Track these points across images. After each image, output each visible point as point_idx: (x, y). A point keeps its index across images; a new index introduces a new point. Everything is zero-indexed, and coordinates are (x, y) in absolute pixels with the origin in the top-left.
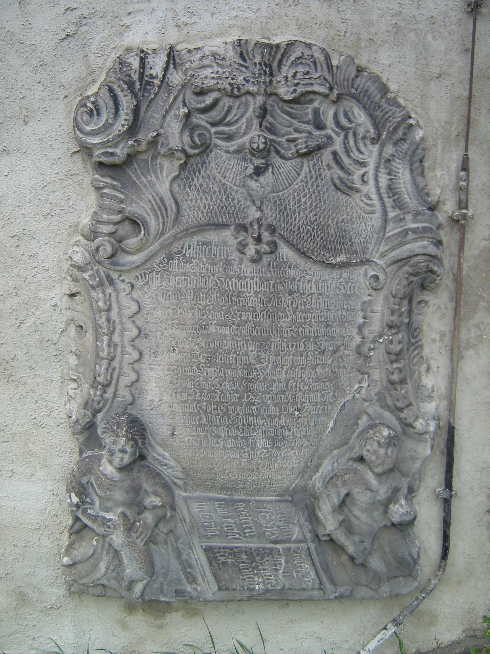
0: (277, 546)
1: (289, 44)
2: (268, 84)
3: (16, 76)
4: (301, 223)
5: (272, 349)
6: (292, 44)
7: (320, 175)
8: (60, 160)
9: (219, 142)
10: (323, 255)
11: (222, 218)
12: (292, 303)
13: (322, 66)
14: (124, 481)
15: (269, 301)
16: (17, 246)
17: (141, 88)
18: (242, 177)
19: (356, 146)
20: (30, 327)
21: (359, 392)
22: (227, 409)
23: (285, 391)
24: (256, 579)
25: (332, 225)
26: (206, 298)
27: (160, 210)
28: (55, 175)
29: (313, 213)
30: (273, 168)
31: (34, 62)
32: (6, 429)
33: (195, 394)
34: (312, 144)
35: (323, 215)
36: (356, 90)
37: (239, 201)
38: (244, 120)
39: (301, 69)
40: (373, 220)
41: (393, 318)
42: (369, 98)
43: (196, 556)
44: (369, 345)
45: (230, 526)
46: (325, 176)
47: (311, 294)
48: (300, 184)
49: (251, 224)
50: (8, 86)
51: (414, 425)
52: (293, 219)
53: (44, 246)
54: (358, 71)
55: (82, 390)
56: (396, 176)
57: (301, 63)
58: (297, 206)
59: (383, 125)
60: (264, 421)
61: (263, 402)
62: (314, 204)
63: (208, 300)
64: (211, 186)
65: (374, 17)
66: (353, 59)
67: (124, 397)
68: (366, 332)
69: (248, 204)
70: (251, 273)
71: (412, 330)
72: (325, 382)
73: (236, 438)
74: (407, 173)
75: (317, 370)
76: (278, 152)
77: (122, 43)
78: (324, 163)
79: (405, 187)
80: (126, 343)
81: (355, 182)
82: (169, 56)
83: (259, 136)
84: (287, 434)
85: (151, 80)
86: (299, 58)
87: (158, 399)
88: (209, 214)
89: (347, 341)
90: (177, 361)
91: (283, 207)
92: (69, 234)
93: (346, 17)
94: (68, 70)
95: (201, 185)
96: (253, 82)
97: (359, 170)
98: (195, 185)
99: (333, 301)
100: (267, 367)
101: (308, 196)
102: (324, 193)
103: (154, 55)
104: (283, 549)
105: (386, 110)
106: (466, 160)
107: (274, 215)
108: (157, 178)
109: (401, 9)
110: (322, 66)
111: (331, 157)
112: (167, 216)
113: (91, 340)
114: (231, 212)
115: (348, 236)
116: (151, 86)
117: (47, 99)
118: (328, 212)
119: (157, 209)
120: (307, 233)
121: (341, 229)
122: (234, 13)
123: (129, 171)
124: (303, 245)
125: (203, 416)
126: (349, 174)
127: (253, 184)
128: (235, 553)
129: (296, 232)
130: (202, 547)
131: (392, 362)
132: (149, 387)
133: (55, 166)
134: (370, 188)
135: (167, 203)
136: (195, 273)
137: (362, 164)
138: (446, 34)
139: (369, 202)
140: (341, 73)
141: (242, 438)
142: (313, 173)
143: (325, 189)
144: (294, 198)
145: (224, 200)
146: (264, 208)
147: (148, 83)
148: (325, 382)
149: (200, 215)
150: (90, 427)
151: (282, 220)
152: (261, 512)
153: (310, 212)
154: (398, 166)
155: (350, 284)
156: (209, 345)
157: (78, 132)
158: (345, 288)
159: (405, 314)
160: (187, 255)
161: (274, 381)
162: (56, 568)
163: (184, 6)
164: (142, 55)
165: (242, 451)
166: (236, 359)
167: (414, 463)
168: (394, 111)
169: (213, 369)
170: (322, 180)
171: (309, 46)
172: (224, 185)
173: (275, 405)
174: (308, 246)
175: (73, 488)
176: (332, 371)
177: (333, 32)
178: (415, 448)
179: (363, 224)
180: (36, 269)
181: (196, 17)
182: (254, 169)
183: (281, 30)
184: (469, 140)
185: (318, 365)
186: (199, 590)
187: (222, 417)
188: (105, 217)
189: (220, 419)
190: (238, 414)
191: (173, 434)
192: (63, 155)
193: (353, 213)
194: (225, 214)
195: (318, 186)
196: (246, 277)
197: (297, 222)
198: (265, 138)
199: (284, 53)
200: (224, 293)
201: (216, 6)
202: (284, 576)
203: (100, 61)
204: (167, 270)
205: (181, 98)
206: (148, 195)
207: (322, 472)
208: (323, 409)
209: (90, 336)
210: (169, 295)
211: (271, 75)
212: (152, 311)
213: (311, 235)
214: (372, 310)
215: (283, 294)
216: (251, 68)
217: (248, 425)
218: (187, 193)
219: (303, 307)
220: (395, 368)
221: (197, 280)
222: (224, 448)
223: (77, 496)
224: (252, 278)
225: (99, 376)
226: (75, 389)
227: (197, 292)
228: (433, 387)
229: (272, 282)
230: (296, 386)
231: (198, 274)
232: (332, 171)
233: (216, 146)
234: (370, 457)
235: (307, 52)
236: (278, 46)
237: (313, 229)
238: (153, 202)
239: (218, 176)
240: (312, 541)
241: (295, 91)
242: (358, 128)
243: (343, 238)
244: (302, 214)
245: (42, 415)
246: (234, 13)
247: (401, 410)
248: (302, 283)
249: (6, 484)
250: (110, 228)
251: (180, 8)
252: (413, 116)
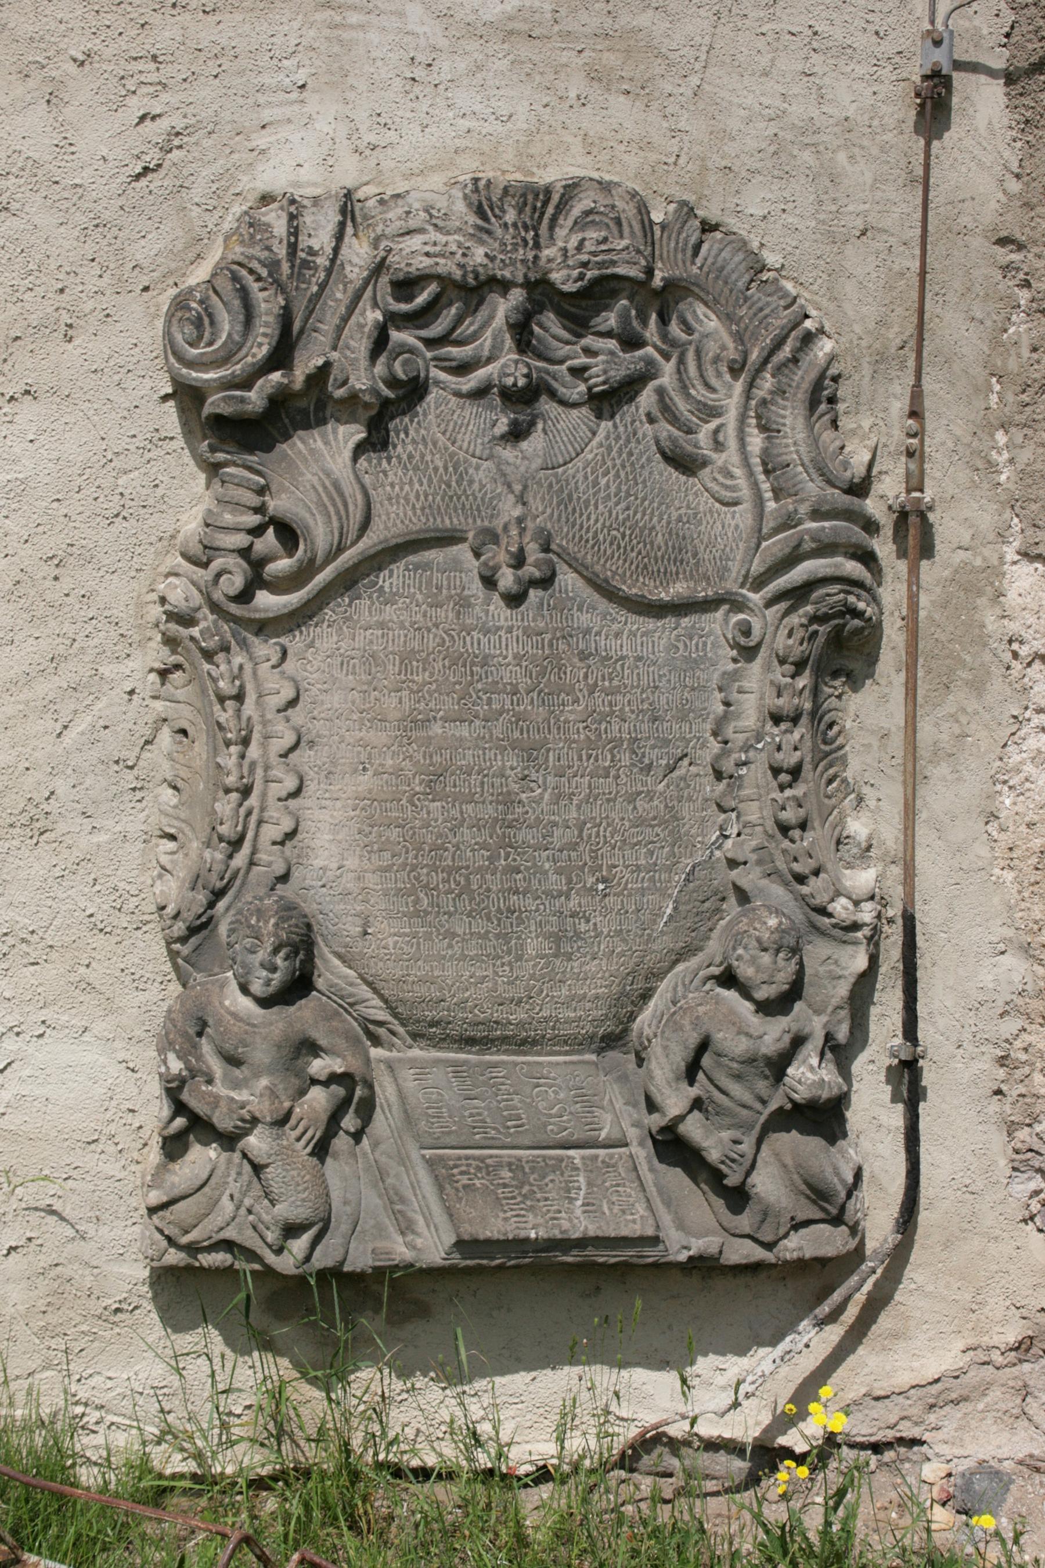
0: (571, 1152)
1: (569, 186)
2: (530, 264)
3: (45, 246)
4: (599, 525)
5: (551, 764)
6: (575, 185)
7: (635, 434)
8: (137, 410)
9: (443, 376)
10: (644, 583)
11: (450, 518)
12: (586, 676)
13: (631, 226)
14: (271, 1024)
15: (542, 673)
16: (56, 578)
17: (292, 273)
18: (486, 440)
19: (702, 376)
20: (83, 733)
21: (719, 848)
22: (468, 879)
23: (577, 844)
24: (531, 1217)
25: (658, 528)
26: (424, 670)
27: (334, 505)
28: (129, 440)
29: (623, 505)
30: (545, 422)
31: (81, 219)
32: (35, 938)
33: (407, 853)
34: (618, 374)
35: (641, 509)
36: (701, 268)
37: (482, 486)
38: (489, 333)
39: (593, 234)
40: (737, 515)
41: (781, 702)
42: (726, 283)
43: (413, 1177)
44: (736, 755)
45: (479, 1114)
46: (645, 436)
47: (622, 658)
48: (595, 451)
49: (506, 528)
50: (31, 266)
51: (830, 908)
52: (584, 517)
53: (108, 576)
54: (704, 231)
55: (186, 855)
56: (779, 431)
57: (592, 222)
58: (591, 492)
59: (753, 334)
60: (538, 902)
61: (535, 865)
62: (624, 488)
63: (427, 674)
64: (428, 458)
65: (734, 124)
66: (692, 209)
67: (269, 864)
68: (729, 732)
69: (499, 491)
70: (506, 619)
71: (823, 726)
72: (653, 826)
73: (485, 936)
74: (800, 423)
75: (638, 803)
76: (553, 394)
77: (252, 185)
78: (641, 410)
79: (797, 452)
80: (274, 759)
81: (702, 444)
82: (343, 211)
83: (516, 362)
84: (583, 927)
85: (310, 258)
86: (588, 213)
87: (335, 866)
88: (427, 511)
89: (694, 748)
90: (370, 791)
91: (564, 495)
92: (157, 553)
93: (679, 127)
94: (150, 236)
95: (410, 457)
96: (502, 261)
97: (707, 422)
98: (398, 457)
99: (665, 671)
100: (542, 798)
101: (613, 472)
102: (643, 467)
103: (314, 209)
104: (583, 1158)
105: (760, 305)
106: (917, 394)
107: (549, 511)
108: (327, 443)
109: (786, 105)
110: (631, 226)
111: (654, 398)
112: (348, 516)
113: (204, 756)
114: (468, 507)
115: (689, 548)
116: (310, 269)
117: (108, 293)
118: (652, 502)
119: (328, 504)
120: (611, 544)
121: (677, 534)
122: (465, 124)
123: (270, 428)
124: (604, 566)
125: (422, 895)
126: (689, 431)
127: (507, 453)
128: (488, 1166)
129: (591, 542)
130: (423, 1156)
131: (782, 788)
132: (317, 843)
133: (128, 422)
134: (731, 456)
135: (347, 491)
136: (402, 622)
137: (711, 412)
138: (875, 151)
139: (729, 482)
140: (669, 238)
141: (498, 936)
142: (621, 429)
143: (644, 460)
144: (586, 478)
145: (454, 484)
146: (529, 497)
147: (305, 264)
148: (653, 826)
149: (410, 513)
150: (200, 927)
151: (563, 519)
152: (538, 1086)
153: (617, 504)
154: (782, 412)
155: (696, 638)
156: (431, 757)
157: (172, 360)
158: (686, 645)
159: (807, 692)
160: (387, 590)
161: (555, 824)
162: (129, 1223)
163: (369, 112)
164: (292, 209)
165: (499, 963)
166: (482, 783)
167: (834, 987)
168: (773, 306)
169: (439, 804)
170: (638, 442)
171: (606, 187)
172: (452, 455)
173: (559, 872)
174: (614, 568)
175: (170, 1044)
176: (666, 806)
177: (653, 157)
178: (835, 957)
179: (719, 524)
180: (94, 622)
181: (392, 132)
182: (509, 425)
183: (554, 157)
184: (925, 354)
185: (639, 793)
186: (419, 1246)
187: (459, 896)
188: (228, 518)
189: (454, 899)
190: (489, 890)
191: (366, 933)
192: (143, 401)
193: (698, 504)
194: (456, 510)
195: (630, 454)
196: (499, 628)
197: (592, 522)
198: (528, 365)
199: (560, 203)
200: (456, 660)
201: (430, 110)
202: (585, 1212)
203: (211, 220)
204: (347, 619)
205: (368, 293)
206: (309, 476)
207: (656, 1005)
208: (652, 880)
209: (200, 749)
210: (354, 666)
211: (537, 246)
212: (321, 697)
213: (619, 548)
214: (740, 687)
215: (569, 660)
216: (499, 232)
217: (509, 910)
218: (385, 473)
219: (607, 683)
220: (788, 798)
221: (406, 636)
222: (463, 957)
223: (179, 1057)
224: (510, 630)
225: (221, 824)
226: (173, 853)
227: (406, 658)
228: (870, 837)
229: (547, 637)
230: (598, 835)
231: (407, 624)
232: (656, 425)
233: (437, 383)
234: (745, 971)
235: (603, 200)
236: (548, 191)
237: (623, 536)
238: (320, 489)
239: (442, 439)
240: (641, 1144)
241: (581, 277)
242: (705, 341)
243: (680, 550)
244: (601, 507)
245: (105, 907)
246: (465, 124)
247: (801, 879)
248: (603, 637)
249: (30, 1051)
250: (241, 540)
251: (362, 116)
252: (813, 313)
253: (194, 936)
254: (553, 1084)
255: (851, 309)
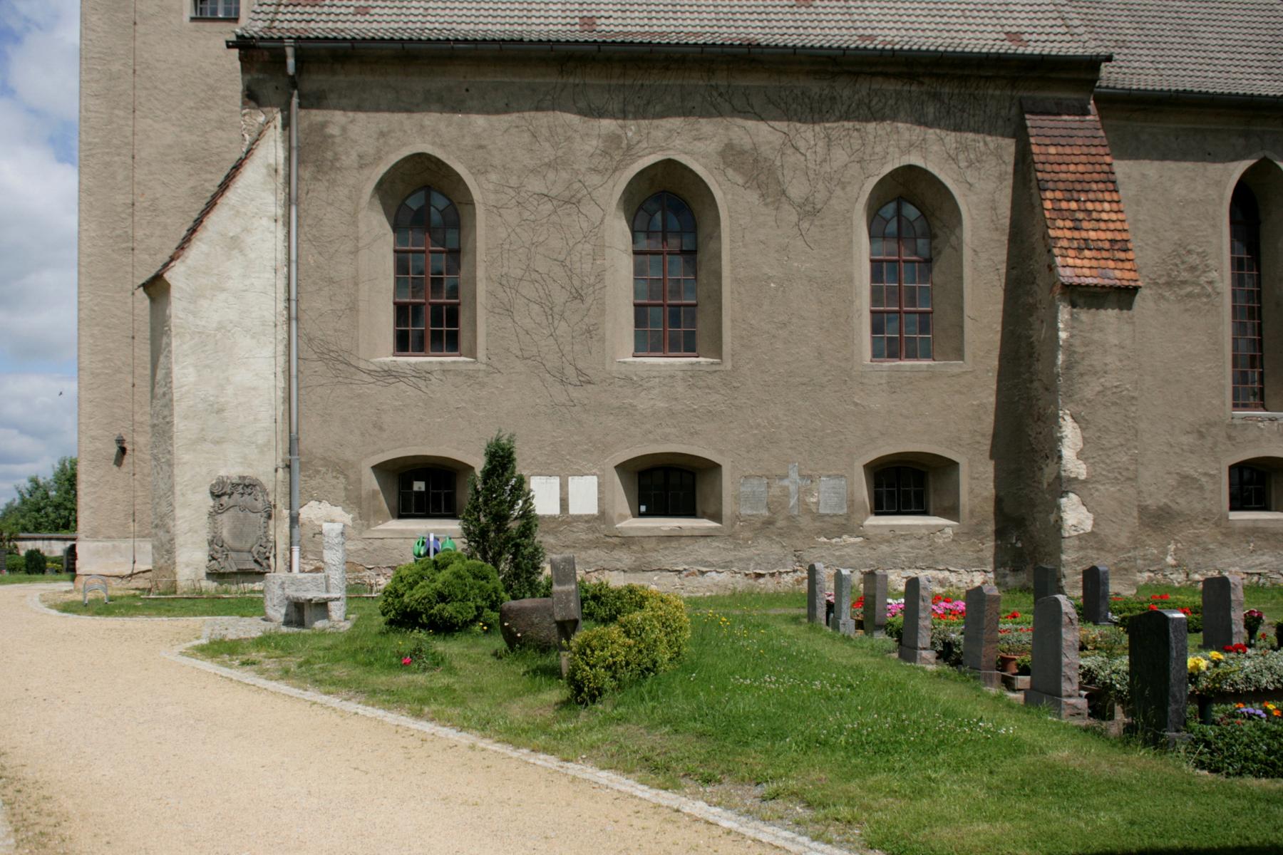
253: (211, 543)
254: (245, 555)
255: (269, 487)
